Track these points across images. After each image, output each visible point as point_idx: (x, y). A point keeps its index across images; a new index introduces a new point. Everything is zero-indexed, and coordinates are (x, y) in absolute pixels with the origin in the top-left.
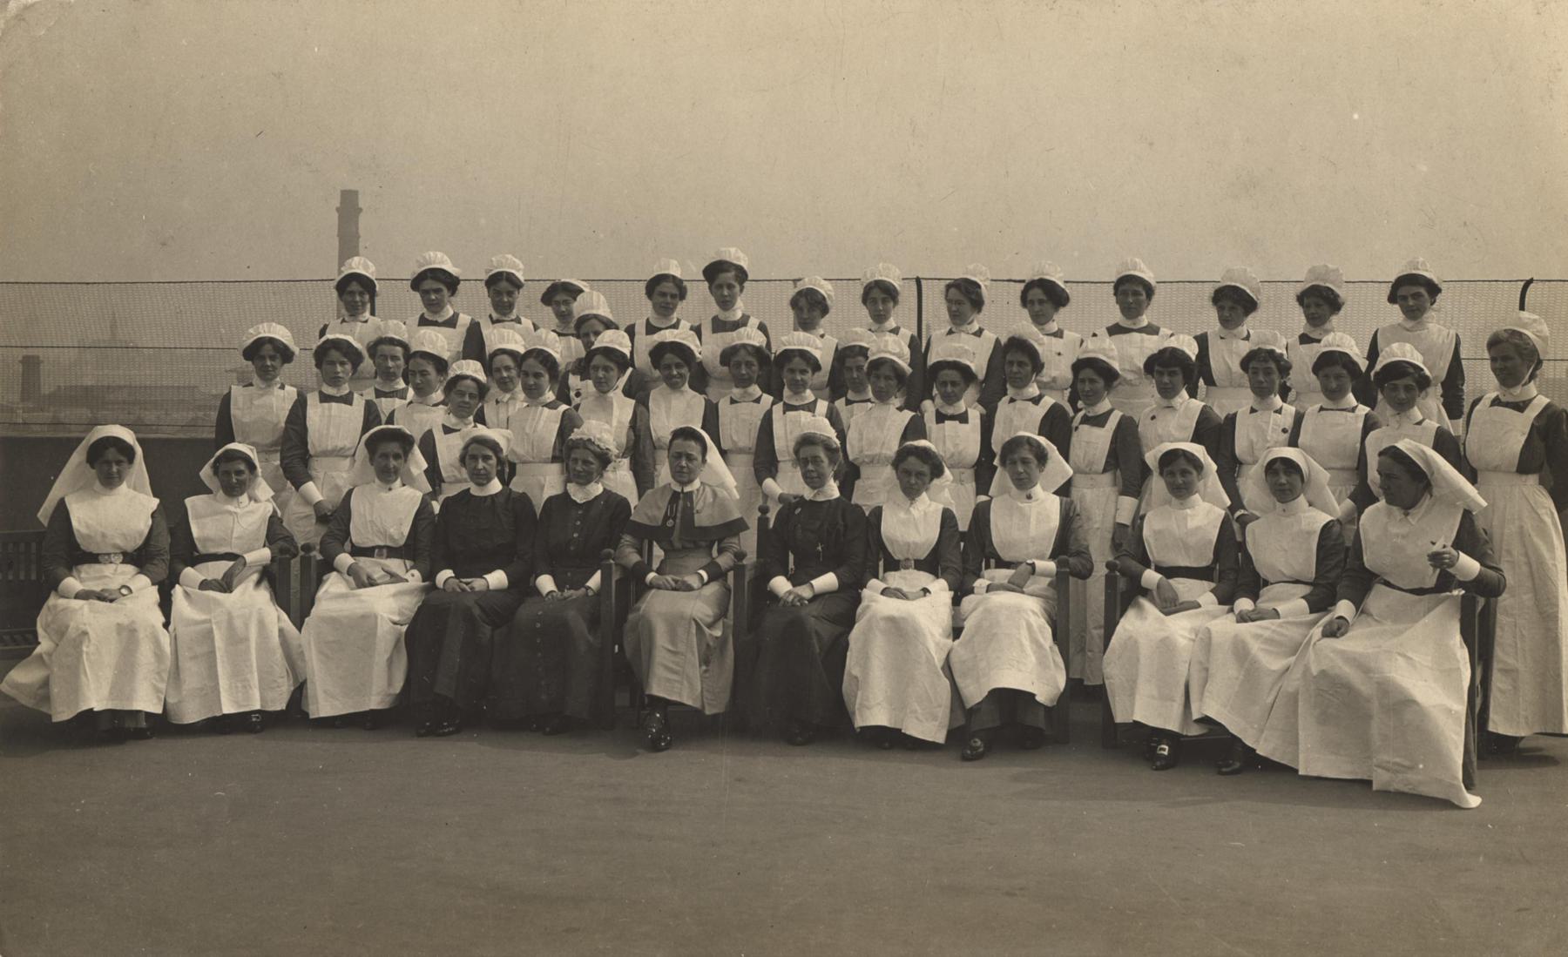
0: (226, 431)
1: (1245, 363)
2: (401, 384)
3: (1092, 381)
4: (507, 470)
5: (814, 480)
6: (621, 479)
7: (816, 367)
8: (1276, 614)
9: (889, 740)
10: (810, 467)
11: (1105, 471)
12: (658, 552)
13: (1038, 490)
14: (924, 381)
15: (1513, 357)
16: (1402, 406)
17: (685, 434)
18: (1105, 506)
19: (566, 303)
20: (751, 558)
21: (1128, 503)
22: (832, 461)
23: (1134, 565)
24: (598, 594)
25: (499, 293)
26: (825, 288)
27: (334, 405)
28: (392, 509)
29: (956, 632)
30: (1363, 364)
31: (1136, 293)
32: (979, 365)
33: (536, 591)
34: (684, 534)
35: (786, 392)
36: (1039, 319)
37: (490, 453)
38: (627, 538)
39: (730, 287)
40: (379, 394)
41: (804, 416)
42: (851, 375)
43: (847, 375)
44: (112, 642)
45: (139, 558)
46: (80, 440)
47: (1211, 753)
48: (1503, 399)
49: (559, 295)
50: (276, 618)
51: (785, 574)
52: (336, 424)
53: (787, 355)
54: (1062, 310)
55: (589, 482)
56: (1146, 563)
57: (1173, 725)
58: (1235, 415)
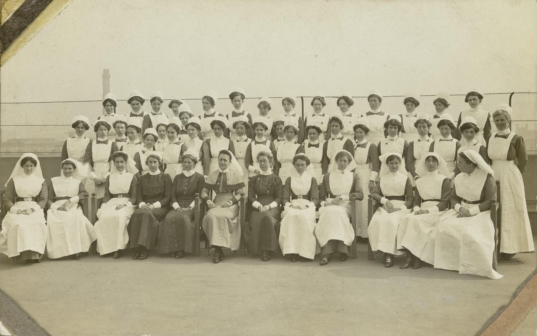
0: (65, 154)
1: (416, 125)
2: (124, 137)
3: (361, 132)
4: (163, 167)
5: (264, 168)
6: (198, 169)
7: (266, 129)
8: (428, 212)
9: (295, 258)
10: (263, 163)
11: (367, 163)
12: (214, 194)
13: (346, 171)
14: (304, 132)
15: (501, 120)
16: (470, 138)
17: (223, 152)
18: (367, 175)
19: (176, 107)
20: (246, 196)
21: (374, 173)
22: (270, 162)
23: (378, 196)
24: (194, 209)
25: (155, 104)
26: (269, 101)
27: (101, 144)
28: (122, 181)
29: (317, 220)
30: (455, 125)
31: (375, 101)
32: (324, 128)
33: (172, 208)
34: (223, 187)
35: (256, 137)
36: (343, 110)
37: (156, 160)
38: (204, 189)
39: (239, 101)
40: (117, 140)
41: (262, 145)
42: (277, 132)
43: (277, 131)
44: (27, 229)
45: (37, 199)
46: (19, 158)
47: (407, 261)
48: (499, 135)
49: (174, 104)
50: (85, 221)
51: (256, 200)
52: (101, 152)
53: (256, 124)
54: (351, 106)
55: (190, 169)
56: (382, 195)
57: (391, 251)
58: (413, 142)
